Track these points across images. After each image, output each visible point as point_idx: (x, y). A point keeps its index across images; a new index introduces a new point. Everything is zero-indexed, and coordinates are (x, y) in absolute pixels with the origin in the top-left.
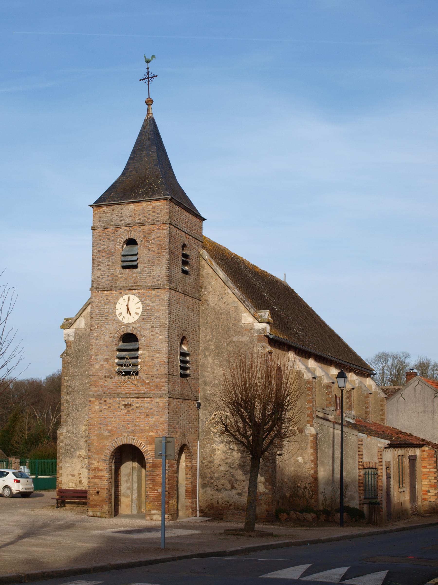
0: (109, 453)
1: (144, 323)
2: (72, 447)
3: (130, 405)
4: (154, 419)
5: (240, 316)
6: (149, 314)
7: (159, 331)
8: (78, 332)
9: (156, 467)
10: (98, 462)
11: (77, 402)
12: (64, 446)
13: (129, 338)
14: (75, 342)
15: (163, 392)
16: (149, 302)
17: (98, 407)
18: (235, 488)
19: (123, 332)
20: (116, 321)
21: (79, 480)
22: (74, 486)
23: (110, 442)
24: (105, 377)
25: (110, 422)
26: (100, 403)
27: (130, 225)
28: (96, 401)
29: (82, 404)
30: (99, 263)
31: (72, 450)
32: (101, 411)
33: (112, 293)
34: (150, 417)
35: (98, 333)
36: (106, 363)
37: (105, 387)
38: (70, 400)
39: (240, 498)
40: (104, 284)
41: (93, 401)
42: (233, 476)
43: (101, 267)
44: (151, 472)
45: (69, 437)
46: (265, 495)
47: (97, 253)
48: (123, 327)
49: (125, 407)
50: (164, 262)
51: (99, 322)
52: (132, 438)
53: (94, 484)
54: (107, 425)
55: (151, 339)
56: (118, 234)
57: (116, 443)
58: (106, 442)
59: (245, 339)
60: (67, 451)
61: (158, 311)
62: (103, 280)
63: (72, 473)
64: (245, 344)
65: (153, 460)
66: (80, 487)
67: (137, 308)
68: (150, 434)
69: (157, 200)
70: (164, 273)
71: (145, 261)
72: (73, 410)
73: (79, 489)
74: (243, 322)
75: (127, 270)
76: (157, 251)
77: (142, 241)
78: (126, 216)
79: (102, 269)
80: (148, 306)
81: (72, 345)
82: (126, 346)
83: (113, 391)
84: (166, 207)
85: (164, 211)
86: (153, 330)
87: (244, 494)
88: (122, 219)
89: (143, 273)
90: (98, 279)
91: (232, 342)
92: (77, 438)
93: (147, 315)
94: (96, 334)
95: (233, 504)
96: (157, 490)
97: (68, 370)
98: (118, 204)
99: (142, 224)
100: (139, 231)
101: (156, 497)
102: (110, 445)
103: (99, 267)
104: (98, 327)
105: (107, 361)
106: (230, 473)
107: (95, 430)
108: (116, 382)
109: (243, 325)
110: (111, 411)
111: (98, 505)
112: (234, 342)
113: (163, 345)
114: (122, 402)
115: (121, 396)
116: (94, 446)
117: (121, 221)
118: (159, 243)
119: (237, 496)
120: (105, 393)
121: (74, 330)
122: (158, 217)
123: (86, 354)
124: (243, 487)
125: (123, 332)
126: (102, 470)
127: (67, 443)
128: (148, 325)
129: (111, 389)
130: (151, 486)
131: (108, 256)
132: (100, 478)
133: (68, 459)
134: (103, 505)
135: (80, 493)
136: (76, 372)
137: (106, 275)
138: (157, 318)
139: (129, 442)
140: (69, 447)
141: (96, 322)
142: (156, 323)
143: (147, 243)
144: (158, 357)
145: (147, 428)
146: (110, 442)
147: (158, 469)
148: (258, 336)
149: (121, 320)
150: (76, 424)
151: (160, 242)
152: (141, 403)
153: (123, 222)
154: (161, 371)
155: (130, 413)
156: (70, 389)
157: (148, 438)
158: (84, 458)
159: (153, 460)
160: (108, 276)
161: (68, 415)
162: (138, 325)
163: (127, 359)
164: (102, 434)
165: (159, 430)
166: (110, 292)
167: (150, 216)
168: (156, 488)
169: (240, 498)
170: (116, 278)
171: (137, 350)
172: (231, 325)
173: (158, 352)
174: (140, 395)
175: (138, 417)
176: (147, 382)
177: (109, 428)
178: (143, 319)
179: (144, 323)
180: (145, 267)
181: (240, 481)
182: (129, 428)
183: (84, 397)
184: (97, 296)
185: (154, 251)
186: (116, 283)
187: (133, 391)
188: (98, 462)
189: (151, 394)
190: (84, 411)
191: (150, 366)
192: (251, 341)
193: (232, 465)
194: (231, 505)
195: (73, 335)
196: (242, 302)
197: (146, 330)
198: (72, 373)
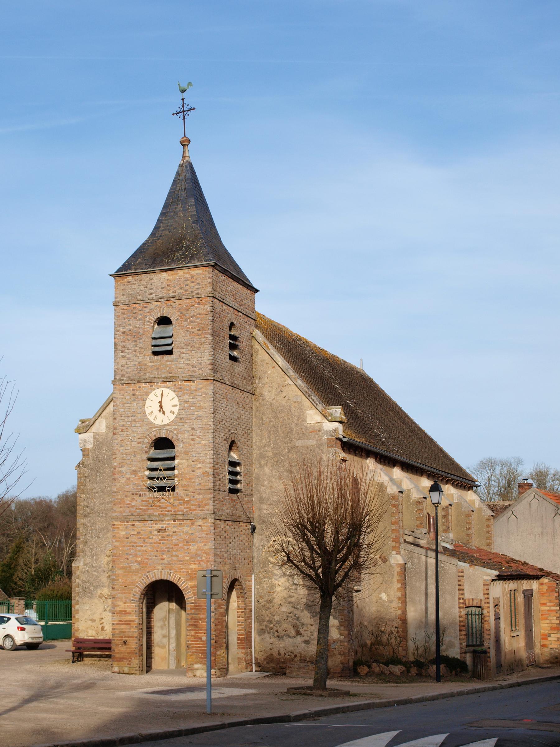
0: (139, 591)
1: (182, 424)
2: (92, 584)
3: (165, 529)
4: (196, 547)
5: (305, 414)
6: (188, 413)
7: (201, 434)
8: (97, 437)
9: (199, 609)
10: (125, 603)
11: (97, 527)
12: (80, 583)
13: (164, 443)
14: (94, 450)
15: (206, 512)
16: (188, 398)
17: (124, 533)
18: (301, 634)
19: (155, 436)
20: (146, 423)
21: (101, 626)
22: (94, 634)
23: (140, 577)
24: (133, 494)
25: (139, 551)
26: (126, 528)
27: (163, 300)
28: (121, 525)
29: (103, 529)
30: (123, 349)
31: (92, 588)
32: (127, 538)
33: (140, 387)
34: (190, 545)
35: (123, 438)
36: (133, 476)
37: (132, 506)
38: (89, 524)
39: (308, 647)
40: (130, 375)
41: (117, 525)
42: (298, 619)
43: (125, 354)
44: (194, 616)
45: (88, 571)
46: (339, 642)
47: (120, 336)
48: (154, 429)
49: (158, 532)
50: (206, 346)
51: (124, 423)
52: (168, 572)
53: (120, 632)
54: (136, 556)
55: (190, 445)
56: (147, 311)
57: (148, 578)
58: (134, 577)
59: (311, 443)
60: (85, 589)
61: (200, 408)
62: (129, 371)
63: (91, 617)
64: (311, 450)
65: (195, 600)
66: (102, 635)
67: (173, 406)
68: (191, 567)
69: (196, 267)
70: (206, 361)
71: (182, 345)
72: (92, 537)
73: (101, 637)
74: (308, 421)
75: (159, 357)
76: (197, 332)
77: (177, 319)
78: (157, 288)
79: (127, 356)
80: (187, 402)
81: (90, 454)
82: (159, 454)
83: (143, 511)
84: (208, 275)
85: (206, 281)
86: (194, 434)
87: (312, 642)
88: (152, 291)
89: (179, 360)
90: (123, 368)
91: (295, 447)
92: (98, 572)
93: (186, 414)
94: (120, 439)
95: (298, 655)
96: (201, 638)
97: (85, 486)
98: (146, 273)
99: (177, 298)
100: (174, 306)
101: (199, 647)
102: (140, 582)
103: (123, 354)
104: (122, 431)
105: (134, 474)
106: (295, 616)
107: (121, 562)
108: (147, 501)
109: (308, 426)
110: (140, 538)
111: (126, 659)
112: (297, 447)
113: (207, 452)
114: (154, 525)
115: (154, 518)
116: (120, 582)
117: (151, 294)
118: (200, 322)
119: (303, 645)
120: (132, 515)
121: (92, 434)
122: (198, 289)
123: (108, 465)
124: (311, 632)
125: (155, 436)
126: (129, 613)
127: (84, 579)
128: (187, 427)
129: (141, 509)
130: (193, 633)
131: (135, 339)
132: (127, 624)
133: (86, 599)
134: (131, 659)
135: (102, 643)
136: (95, 488)
137: (133, 363)
138: (199, 417)
139: (164, 577)
140: (88, 584)
141: (120, 423)
142: (197, 424)
143: (185, 323)
144: (200, 468)
145: (188, 558)
146: (140, 577)
147: (201, 612)
148: (328, 439)
149: (153, 421)
150: (97, 555)
151: (201, 320)
152: (179, 527)
153: (154, 295)
154: (204, 486)
155: (165, 540)
156: (88, 510)
157: (188, 572)
158: (106, 598)
159: (195, 600)
160: (135, 365)
161: (85, 543)
162: (173, 427)
163: (161, 470)
164: (130, 567)
165: (202, 561)
166: (137, 385)
167: (187, 288)
168: (200, 635)
169: (308, 647)
170: (146, 367)
171: (173, 459)
172: (293, 425)
173: (200, 461)
174: (177, 516)
175: (176, 545)
176: (186, 499)
177: (139, 559)
178: (180, 419)
179: (182, 424)
180: (182, 353)
181: (307, 625)
182: (164, 559)
183: (106, 520)
184: (121, 390)
185: (193, 332)
186: (145, 373)
187: (168, 511)
188: (125, 603)
189: (192, 515)
190: (106, 538)
191: (190, 479)
192: (319, 446)
193: (297, 605)
194: (296, 656)
195: (92, 441)
196: (307, 396)
197: (185, 433)
198: (90, 490)
